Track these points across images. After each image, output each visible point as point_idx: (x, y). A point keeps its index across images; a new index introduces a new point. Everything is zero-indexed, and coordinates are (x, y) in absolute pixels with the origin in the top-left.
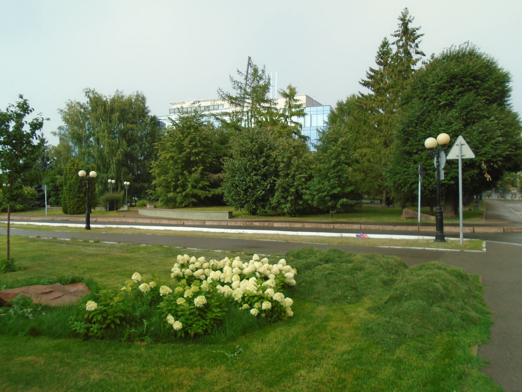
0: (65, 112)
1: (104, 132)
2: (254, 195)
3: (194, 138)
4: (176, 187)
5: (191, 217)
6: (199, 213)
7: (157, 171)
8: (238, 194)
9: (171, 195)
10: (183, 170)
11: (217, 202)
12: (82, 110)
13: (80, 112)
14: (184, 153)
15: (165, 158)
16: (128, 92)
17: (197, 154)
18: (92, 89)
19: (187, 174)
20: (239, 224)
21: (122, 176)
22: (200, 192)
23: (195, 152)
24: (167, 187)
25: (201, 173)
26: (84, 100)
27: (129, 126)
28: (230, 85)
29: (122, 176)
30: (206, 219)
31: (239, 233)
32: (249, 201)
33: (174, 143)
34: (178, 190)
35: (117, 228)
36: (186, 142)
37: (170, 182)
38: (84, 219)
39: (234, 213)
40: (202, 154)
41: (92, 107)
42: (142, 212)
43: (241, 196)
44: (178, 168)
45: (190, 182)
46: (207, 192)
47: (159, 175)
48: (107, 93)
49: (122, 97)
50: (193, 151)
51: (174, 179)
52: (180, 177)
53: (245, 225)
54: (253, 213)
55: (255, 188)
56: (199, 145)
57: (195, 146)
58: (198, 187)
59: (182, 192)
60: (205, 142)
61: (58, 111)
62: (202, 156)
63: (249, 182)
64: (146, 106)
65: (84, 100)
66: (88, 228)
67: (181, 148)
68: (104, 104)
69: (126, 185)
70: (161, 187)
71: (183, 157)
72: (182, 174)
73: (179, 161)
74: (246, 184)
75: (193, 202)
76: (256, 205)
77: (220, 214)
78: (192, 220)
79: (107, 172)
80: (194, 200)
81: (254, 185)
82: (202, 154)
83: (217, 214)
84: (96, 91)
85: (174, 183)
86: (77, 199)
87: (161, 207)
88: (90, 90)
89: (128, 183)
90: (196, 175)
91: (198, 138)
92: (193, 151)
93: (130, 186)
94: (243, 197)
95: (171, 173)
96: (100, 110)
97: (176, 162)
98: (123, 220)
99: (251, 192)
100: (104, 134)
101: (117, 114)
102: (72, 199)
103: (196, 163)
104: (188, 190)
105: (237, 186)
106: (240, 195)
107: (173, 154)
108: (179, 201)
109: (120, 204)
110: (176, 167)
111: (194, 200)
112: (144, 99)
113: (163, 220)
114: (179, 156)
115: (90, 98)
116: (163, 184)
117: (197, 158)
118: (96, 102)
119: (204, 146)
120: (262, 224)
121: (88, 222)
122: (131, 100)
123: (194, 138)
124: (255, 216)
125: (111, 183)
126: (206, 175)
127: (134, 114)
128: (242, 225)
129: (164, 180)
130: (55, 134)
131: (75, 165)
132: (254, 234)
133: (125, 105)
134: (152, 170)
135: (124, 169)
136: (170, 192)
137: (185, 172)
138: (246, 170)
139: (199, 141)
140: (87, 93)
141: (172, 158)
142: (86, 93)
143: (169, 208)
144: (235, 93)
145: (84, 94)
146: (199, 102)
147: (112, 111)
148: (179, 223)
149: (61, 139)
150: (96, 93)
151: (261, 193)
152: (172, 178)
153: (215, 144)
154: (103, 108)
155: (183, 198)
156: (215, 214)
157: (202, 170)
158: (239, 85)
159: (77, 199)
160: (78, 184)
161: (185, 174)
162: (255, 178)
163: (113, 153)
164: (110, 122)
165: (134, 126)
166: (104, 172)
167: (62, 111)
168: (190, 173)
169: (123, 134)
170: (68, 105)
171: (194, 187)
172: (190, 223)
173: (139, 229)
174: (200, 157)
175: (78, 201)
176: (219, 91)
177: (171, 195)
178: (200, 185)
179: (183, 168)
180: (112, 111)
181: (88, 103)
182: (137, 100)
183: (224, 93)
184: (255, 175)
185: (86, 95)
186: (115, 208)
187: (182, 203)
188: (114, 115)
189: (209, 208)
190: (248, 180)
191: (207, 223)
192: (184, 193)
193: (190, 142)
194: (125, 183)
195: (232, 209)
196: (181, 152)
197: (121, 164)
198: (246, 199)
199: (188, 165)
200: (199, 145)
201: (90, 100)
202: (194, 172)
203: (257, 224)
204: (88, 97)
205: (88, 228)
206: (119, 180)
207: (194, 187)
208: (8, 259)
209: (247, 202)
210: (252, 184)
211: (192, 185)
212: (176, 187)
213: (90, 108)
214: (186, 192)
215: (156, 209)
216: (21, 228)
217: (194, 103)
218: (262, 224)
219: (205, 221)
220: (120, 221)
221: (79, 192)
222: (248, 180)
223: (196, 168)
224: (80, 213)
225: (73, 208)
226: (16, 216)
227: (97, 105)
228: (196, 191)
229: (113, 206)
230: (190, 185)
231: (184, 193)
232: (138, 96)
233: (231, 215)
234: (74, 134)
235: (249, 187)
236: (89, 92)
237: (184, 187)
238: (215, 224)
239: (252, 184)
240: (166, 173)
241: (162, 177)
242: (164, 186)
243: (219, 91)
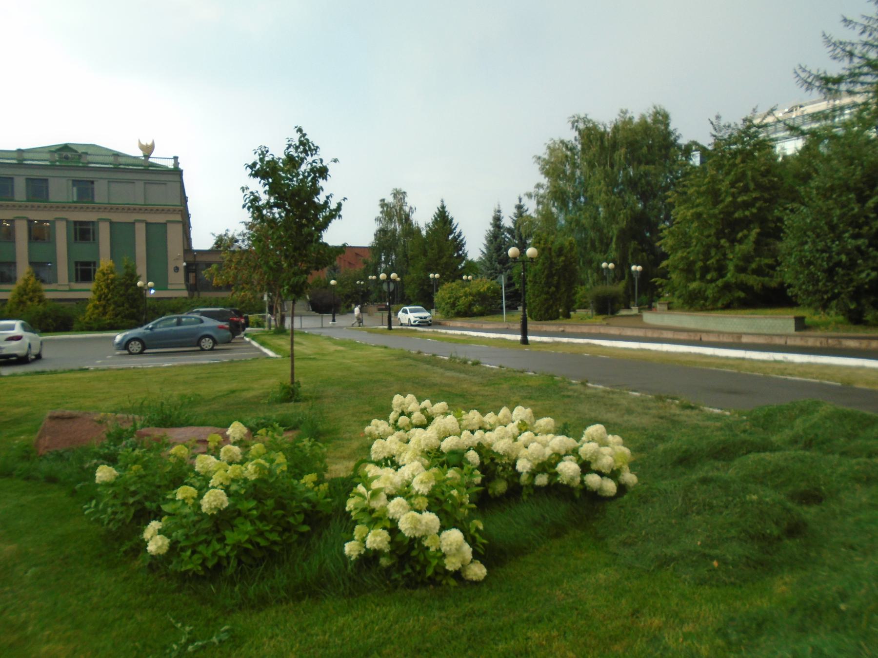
0: (544, 159)
1: (600, 183)
2: (851, 280)
3: (744, 174)
4: (706, 270)
5: (721, 328)
6: (735, 320)
7: (670, 242)
8: (813, 279)
9: (694, 285)
10: (718, 239)
11: (773, 298)
12: (569, 153)
13: (567, 156)
14: (721, 206)
15: (684, 219)
16: (639, 109)
17: (746, 205)
18: (582, 116)
19: (727, 245)
20: (810, 342)
21: (630, 257)
22: (753, 280)
23: (744, 202)
24: (689, 271)
25: (757, 242)
26: (571, 136)
27: (643, 168)
28: (826, 52)
29: (630, 257)
30: (745, 330)
31: (776, 362)
32: (840, 293)
33: (703, 189)
34: (709, 277)
35: (568, 343)
36: (724, 186)
37: (694, 262)
38: (518, 326)
39: (808, 321)
40: (757, 205)
41: (582, 144)
42: (649, 317)
43: (820, 284)
44: (708, 236)
45: (731, 260)
46: (767, 279)
47: (674, 249)
48: (606, 118)
49: (631, 119)
50: (739, 200)
51: (701, 257)
52: (713, 252)
53: (824, 345)
54: (856, 319)
55: (852, 265)
56: (752, 186)
57: (746, 190)
58: (750, 269)
59: (717, 280)
60: (765, 181)
61: (534, 160)
62: (760, 209)
63: (839, 254)
64: (671, 127)
65: (571, 136)
66: (525, 341)
67: (715, 195)
68: (603, 135)
69: (636, 271)
70: (677, 272)
71: (720, 213)
72: (718, 247)
73: (712, 222)
74: (830, 257)
75: (739, 298)
76: (859, 304)
77: (778, 322)
78: (765, 335)
79: (605, 252)
80: (742, 295)
81: (850, 260)
82: (757, 205)
83: (771, 321)
84: (589, 117)
85: (700, 264)
86: (545, 296)
87: (681, 308)
88: (579, 118)
89: (639, 268)
90: (747, 247)
91: (749, 173)
92: (739, 200)
93: (642, 273)
94: (825, 285)
95: (696, 247)
96: (595, 149)
97: (705, 225)
98: (603, 330)
99: (844, 275)
100: (599, 188)
101: (623, 151)
102: (537, 296)
103: (745, 223)
104: (729, 275)
105: (810, 263)
106: (818, 281)
107: (700, 209)
108: (711, 296)
109: (617, 305)
110: (706, 233)
111: (742, 295)
112: (666, 116)
113: (663, 332)
114: (712, 211)
115: (580, 131)
116: (681, 266)
117: (747, 213)
118: (590, 135)
119: (759, 187)
120: (864, 344)
121: (524, 332)
122: (646, 122)
123: (744, 174)
124: (858, 327)
125: (607, 268)
126: (767, 245)
127: (650, 147)
128: (818, 344)
129: (682, 258)
130: (530, 196)
131: (542, 242)
132: (810, 365)
133: (636, 133)
134: (662, 241)
135: (633, 244)
136: (694, 280)
137: (723, 241)
138: (833, 228)
139: (753, 179)
140: (574, 123)
141: (698, 216)
142: (573, 123)
143: (696, 310)
144: (835, 69)
145: (570, 125)
146: (801, 107)
147: (614, 146)
148: (692, 338)
149: (538, 203)
150: (589, 121)
151: (868, 275)
152: (698, 254)
153: (789, 181)
154: (599, 143)
155: (719, 292)
156: (766, 321)
157: (759, 234)
158: (848, 48)
159: (545, 296)
160: (546, 272)
161: (722, 247)
162: (851, 243)
163: (612, 217)
164: (612, 166)
165: (651, 168)
166: (601, 252)
167: (539, 158)
168: (733, 241)
169: (632, 184)
170: (549, 147)
171: (741, 270)
172: (713, 338)
173: (600, 346)
174: (754, 210)
175: (546, 300)
176: (799, 72)
177: (694, 285)
178: (754, 266)
179: (719, 234)
180: (614, 146)
181: (576, 140)
182: (656, 121)
183: (810, 74)
184: (855, 237)
185: (573, 126)
186: (609, 310)
187: (716, 300)
188: (617, 153)
189: (759, 311)
190: (835, 247)
191: (745, 340)
192: (720, 283)
193: (733, 185)
194: (633, 268)
195: (807, 314)
196: (716, 203)
197: (625, 236)
198: (833, 289)
199: (730, 227)
200: (752, 186)
201: (580, 134)
202: (740, 241)
203: (852, 344)
204: (577, 129)
205: (525, 341)
206: (623, 265)
207: (741, 270)
208: (293, 383)
209: (835, 297)
210: (844, 258)
211: (736, 266)
212: (706, 270)
213: (579, 147)
214: (725, 279)
215: (670, 312)
216: (446, 339)
217: (791, 111)
218: (864, 344)
219: (740, 335)
220: (598, 332)
221: (548, 284)
222: (835, 247)
223: (745, 232)
224: (551, 319)
225: (539, 310)
226: (549, 325)
227: (591, 141)
228: (743, 277)
229: (606, 307)
230: (731, 267)
231: (720, 283)
232: (657, 113)
233: (801, 324)
234: (556, 192)
235: (839, 264)
236: (577, 121)
237: (721, 270)
238: (761, 340)
239: (844, 258)
240: (687, 245)
241: (680, 254)
242: (682, 270)
243: (799, 72)
